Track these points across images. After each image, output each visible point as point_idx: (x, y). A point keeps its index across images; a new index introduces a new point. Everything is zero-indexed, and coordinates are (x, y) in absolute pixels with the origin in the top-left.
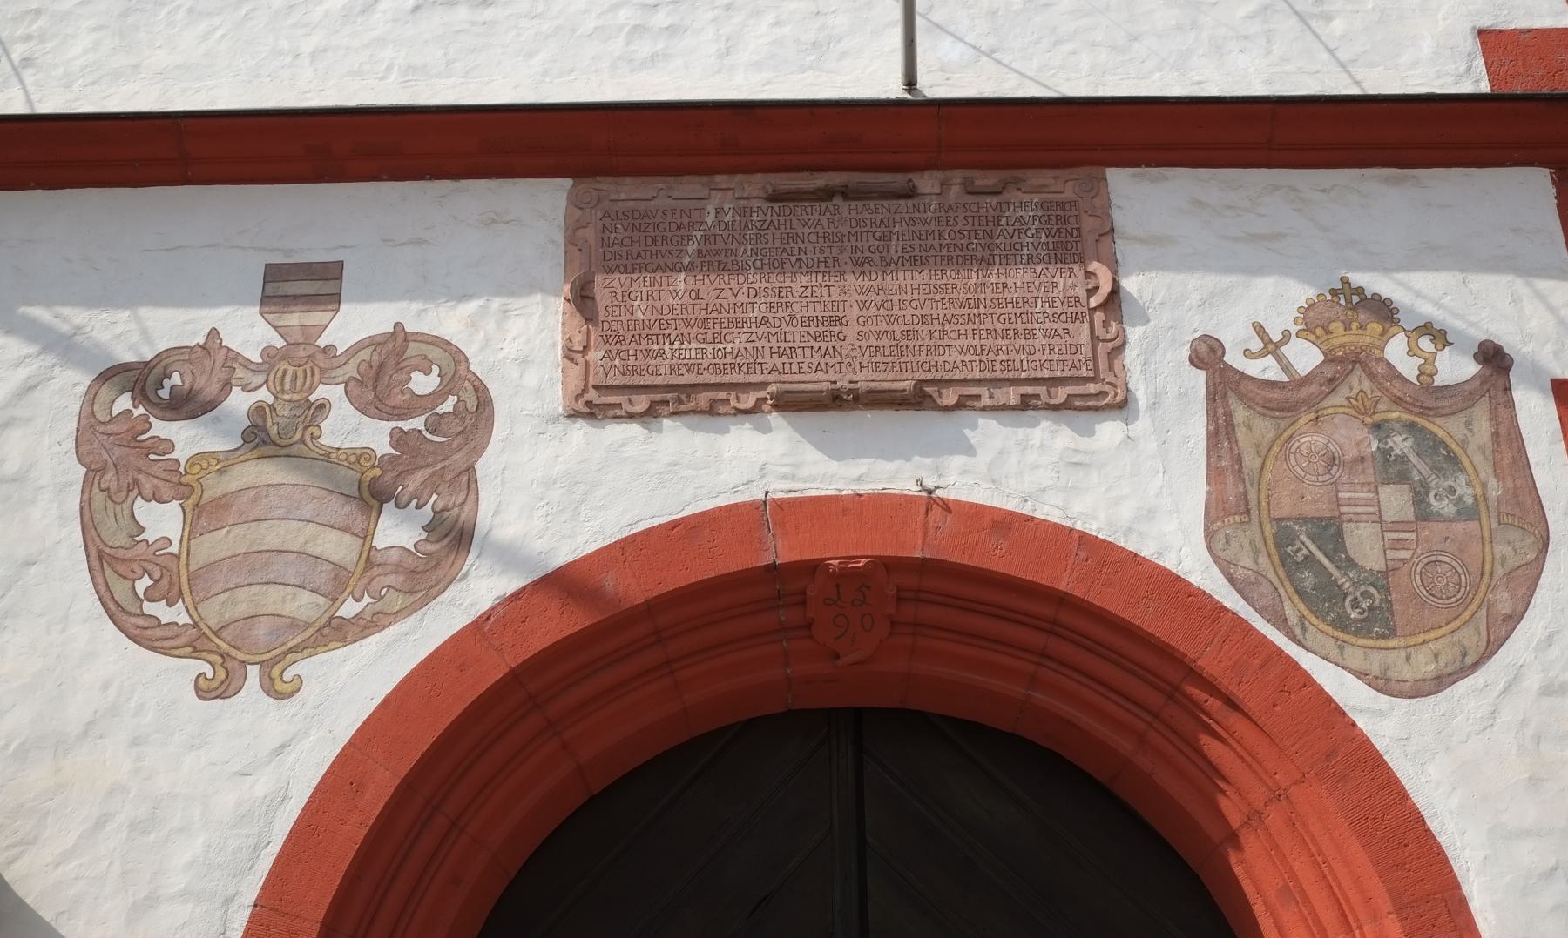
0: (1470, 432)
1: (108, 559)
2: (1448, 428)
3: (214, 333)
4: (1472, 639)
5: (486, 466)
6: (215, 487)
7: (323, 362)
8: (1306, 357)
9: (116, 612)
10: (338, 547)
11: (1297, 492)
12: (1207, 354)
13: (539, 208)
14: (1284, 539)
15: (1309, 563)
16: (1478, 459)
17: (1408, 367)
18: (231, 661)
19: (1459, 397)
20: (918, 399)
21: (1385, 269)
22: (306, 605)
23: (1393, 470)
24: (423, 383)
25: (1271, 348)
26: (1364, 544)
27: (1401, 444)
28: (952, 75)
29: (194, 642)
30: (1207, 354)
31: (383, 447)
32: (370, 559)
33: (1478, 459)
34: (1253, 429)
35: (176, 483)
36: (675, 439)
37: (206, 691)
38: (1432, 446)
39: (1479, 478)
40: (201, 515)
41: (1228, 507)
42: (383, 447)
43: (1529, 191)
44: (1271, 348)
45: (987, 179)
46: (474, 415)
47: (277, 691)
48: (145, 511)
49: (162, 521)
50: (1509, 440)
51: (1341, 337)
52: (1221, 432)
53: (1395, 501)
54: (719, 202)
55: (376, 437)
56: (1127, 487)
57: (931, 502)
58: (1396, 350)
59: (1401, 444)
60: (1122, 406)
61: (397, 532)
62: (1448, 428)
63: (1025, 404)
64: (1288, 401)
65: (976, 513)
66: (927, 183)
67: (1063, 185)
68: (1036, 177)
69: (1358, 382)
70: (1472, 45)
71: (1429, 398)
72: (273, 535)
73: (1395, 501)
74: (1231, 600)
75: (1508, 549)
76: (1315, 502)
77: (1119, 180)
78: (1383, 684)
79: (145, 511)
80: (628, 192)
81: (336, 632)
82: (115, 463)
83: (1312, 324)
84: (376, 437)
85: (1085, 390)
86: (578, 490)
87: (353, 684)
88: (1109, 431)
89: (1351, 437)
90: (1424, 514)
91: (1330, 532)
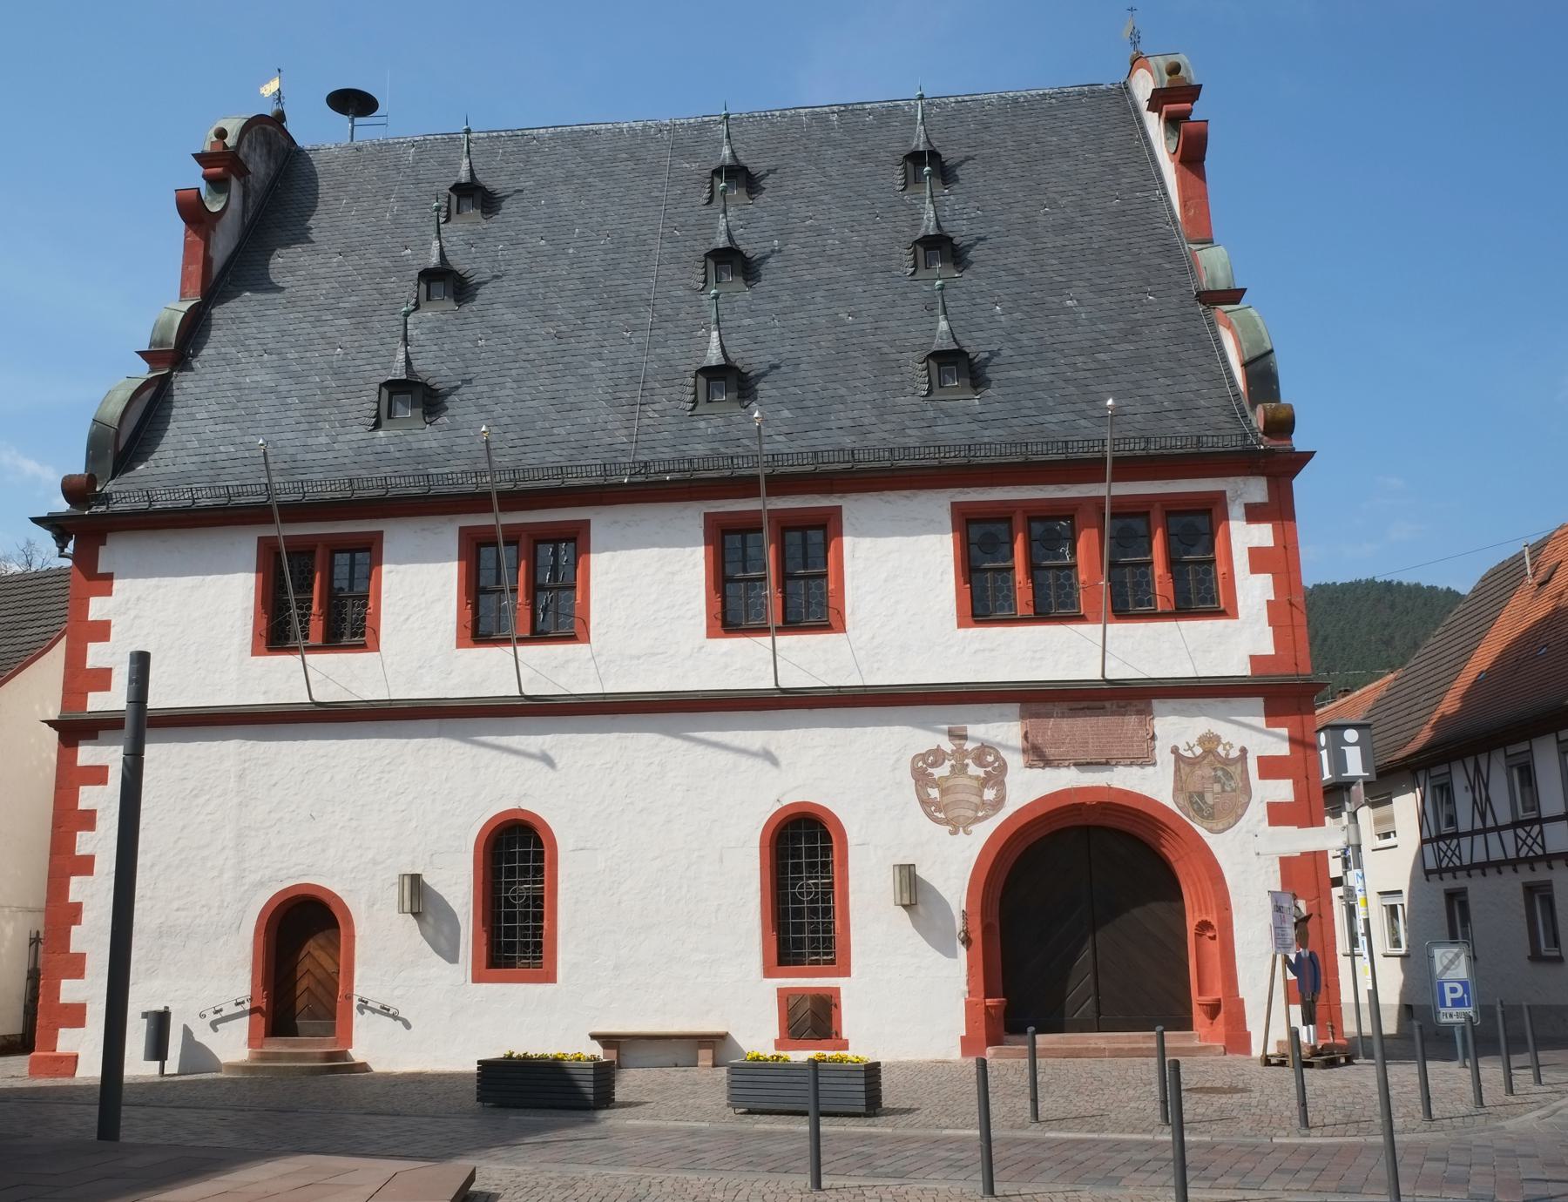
0: (1235, 770)
1: (925, 802)
2: (1231, 769)
3: (1210, 742)
4: (1231, 821)
5: (1007, 780)
6: (945, 785)
7: (965, 754)
8: (1198, 751)
9: (929, 815)
11: (1194, 785)
12: (1175, 750)
13: (1015, 708)
14: (1191, 797)
15: (1196, 802)
16: (1237, 777)
17: (1223, 754)
18: (957, 825)
19: (1235, 761)
20: (1107, 763)
21: (952, 918)
22: (970, 813)
23: (1217, 780)
24: (990, 759)
25: (1190, 748)
26: (1209, 798)
27: (1220, 773)
28: (1116, 672)
29: (947, 822)
30: (1175, 750)
31: (983, 775)
32: (983, 803)
33: (1237, 777)
34: (1185, 769)
36: (1049, 772)
37: (952, 833)
38: (1226, 773)
39: (1237, 782)
40: (943, 792)
41: (1179, 788)
42: (983, 775)
43: (1258, 703)
44: (1190, 748)
45: (1122, 703)
46: (1003, 767)
47: (967, 833)
48: (930, 790)
49: (934, 793)
50: (1245, 771)
51: (1207, 745)
52: (1177, 770)
53: (1217, 788)
54: (1059, 707)
55: (981, 772)
56: (1153, 784)
57: (965, 915)
58: (1220, 749)
59: (1220, 773)
60: (1154, 764)
61: (989, 794)
62: (1231, 769)
63: (1132, 764)
64: (1194, 762)
65: (1120, 791)
68: (1135, 702)
69: (1211, 757)
70: (1248, 660)
71: (1227, 761)
72: (960, 797)
73: (1217, 788)
74: (1178, 812)
75: (1243, 799)
76: (1199, 788)
78: (1211, 831)
79: (930, 790)
81: (977, 820)
82: (921, 777)
83: (1202, 741)
84: (981, 772)
86: (1028, 786)
87: (984, 831)
88: (1150, 770)
89: (1208, 772)
90: (1224, 791)
91: (1201, 795)
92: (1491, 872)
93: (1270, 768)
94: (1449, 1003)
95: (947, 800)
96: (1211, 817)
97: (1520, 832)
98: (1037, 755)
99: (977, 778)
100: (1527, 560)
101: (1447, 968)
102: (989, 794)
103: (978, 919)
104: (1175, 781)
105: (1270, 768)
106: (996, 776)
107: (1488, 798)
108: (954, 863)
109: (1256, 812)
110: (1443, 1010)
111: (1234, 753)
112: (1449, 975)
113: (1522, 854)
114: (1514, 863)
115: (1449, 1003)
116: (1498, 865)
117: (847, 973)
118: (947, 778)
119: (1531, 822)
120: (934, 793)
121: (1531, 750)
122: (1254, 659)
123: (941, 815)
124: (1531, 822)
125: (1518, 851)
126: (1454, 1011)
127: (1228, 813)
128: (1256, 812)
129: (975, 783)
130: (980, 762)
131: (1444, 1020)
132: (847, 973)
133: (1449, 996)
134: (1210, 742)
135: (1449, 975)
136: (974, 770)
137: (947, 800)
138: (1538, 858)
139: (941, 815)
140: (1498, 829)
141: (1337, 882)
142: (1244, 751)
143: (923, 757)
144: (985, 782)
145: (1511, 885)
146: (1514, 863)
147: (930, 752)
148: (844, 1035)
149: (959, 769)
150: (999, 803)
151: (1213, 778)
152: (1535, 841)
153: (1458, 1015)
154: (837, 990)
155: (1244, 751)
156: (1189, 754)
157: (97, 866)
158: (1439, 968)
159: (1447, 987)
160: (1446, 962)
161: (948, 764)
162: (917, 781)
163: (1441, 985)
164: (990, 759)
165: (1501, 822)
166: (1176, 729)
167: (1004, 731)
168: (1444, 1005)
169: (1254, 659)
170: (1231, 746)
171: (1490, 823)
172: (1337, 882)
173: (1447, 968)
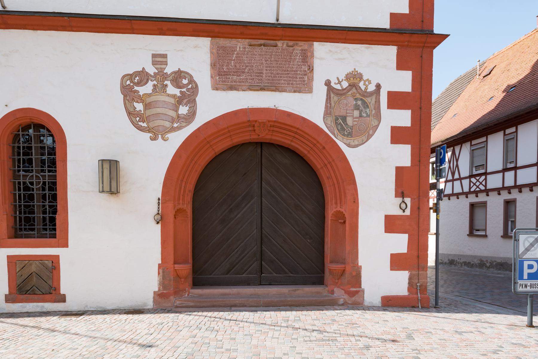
0: (371, 101)
1: (131, 114)
2: (368, 100)
3: (354, 78)
7: (165, 76)
8: (345, 84)
10: (173, 114)
12: (328, 83)
14: (337, 119)
15: (340, 123)
16: (372, 106)
17: (363, 88)
18: (156, 133)
19: (371, 94)
22: (168, 124)
23: (357, 107)
24: (185, 82)
27: (359, 103)
30: (328, 83)
32: (178, 116)
33: (372, 106)
34: (334, 98)
35: (141, 99)
37: (152, 139)
38: (364, 103)
40: (147, 106)
41: (328, 112)
44: (339, 83)
45: (291, 43)
46: (195, 90)
47: (165, 140)
48: (136, 104)
49: (139, 107)
50: (378, 102)
53: (356, 113)
55: (177, 92)
56: (309, 106)
58: (361, 85)
61: (183, 110)
64: (341, 93)
66: (280, 43)
67: (304, 45)
69: (354, 90)
71: (366, 94)
72: (159, 110)
73: (356, 113)
75: (374, 123)
76: (343, 113)
77: (316, 44)
78: (349, 146)
79: (136, 104)
80: (223, 42)
81: (173, 130)
82: (128, 92)
83: (348, 77)
84: (177, 92)
85: (303, 85)
86: (215, 104)
87: (177, 139)
89: (351, 102)
90: (361, 116)
91: (344, 119)
92: (453, 198)
93: (397, 100)
94: (525, 277)
95: (149, 112)
96: (350, 135)
97: (473, 180)
98: (225, 77)
99: (174, 96)
100: (478, 69)
101: (527, 250)
102: (183, 110)
103: (170, 205)
104: (326, 107)
105: (397, 100)
106: (189, 96)
107: (457, 166)
108: (150, 161)
109: (383, 133)
110: (520, 282)
111: (372, 88)
112: (528, 255)
113: (472, 190)
114: (466, 194)
115: (525, 277)
116: (458, 195)
117: (66, 245)
118: (149, 95)
119: (480, 175)
120: (139, 107)
121: (487, 141)
122: (393, 16)
123: (145, 125)
124: (480, 175)
125: (470, 188)
126: (529, 283)
127: (362, 133)
128: (383, 133)
129: (172, 101)
130: (177, 84)
131: (520, 289)
132: (66, 245)
133: (526, 271)
134: (354, 78)
135: (528, 255)
136: (172, 90)
137: (149, 112)
138: (481, 191)
139: (145, 125)
140: (460, 179)
141: (434, 186)
142: (378, 86)
143: (131, 77)
144: (180, 101)
145: (464, 203)
146: (466, 194)
147: (137, 73)
148: (62, 292)
149: (160, 88)
150: (191, 116)
151: (353, 100)
152: (481, 183)
153: (531, 286)
154: (58, 257)
155: (378, 86)
156: (338, 87)
157: (475, 242)
158: (521, 249)
159: (526, 264)
160: (527, 245)
161: (150, 84)
162: (125, 96)
163: (522, 263)
164: (185, 82)
165: (462, 176)
166: (331, 63)
167: (193, 56)
168: (521, 278)
169: (393, 16)
170: (370, 82)
171: (456, 176)
172: (434, 186)
173: (527, 250)
